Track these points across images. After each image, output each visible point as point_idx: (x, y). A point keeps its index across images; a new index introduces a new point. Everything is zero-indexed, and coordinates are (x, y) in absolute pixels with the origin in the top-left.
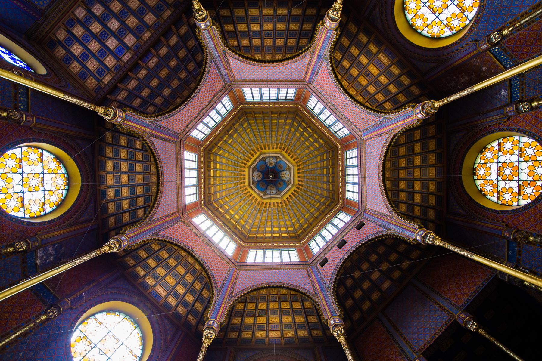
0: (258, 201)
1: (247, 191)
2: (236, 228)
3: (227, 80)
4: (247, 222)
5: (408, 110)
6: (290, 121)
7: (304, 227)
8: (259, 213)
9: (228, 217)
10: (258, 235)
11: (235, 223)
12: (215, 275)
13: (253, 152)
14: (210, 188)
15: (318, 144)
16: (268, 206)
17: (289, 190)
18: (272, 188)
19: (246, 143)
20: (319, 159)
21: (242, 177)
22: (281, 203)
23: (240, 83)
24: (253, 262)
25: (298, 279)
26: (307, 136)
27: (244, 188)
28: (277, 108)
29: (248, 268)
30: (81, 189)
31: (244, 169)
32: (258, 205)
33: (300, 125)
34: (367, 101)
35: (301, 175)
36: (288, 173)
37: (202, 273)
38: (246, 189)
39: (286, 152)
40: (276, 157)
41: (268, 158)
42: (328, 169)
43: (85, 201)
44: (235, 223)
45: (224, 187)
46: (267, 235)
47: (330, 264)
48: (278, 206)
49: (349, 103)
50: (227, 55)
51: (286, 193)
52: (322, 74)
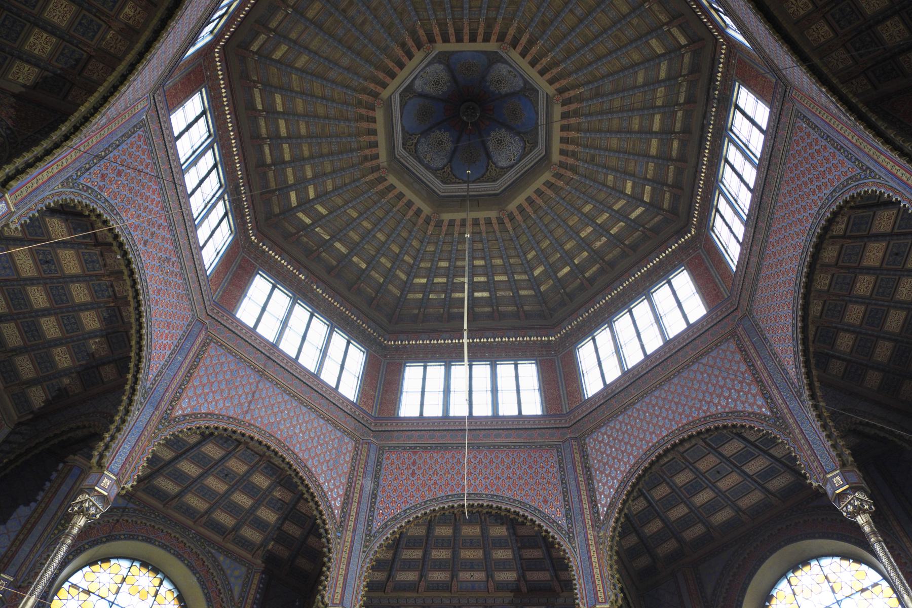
0: (566, 108)
2: (690, 100)
3: (372, 456)
4: (652, 83)
8: (598, 74)
11: (680, 114)
16: (555, 71)
18: (499, 82)
20: (302, 61)
22: (514, 44)
23: (350, 424)
26: (286, 146)
30: (802, 539)
32: (579, 99)
35: (391, 65)
36: (418, 83)
43: (823, 519)
44: (680, 114)
48: (531, 43)
50: (338, 520)
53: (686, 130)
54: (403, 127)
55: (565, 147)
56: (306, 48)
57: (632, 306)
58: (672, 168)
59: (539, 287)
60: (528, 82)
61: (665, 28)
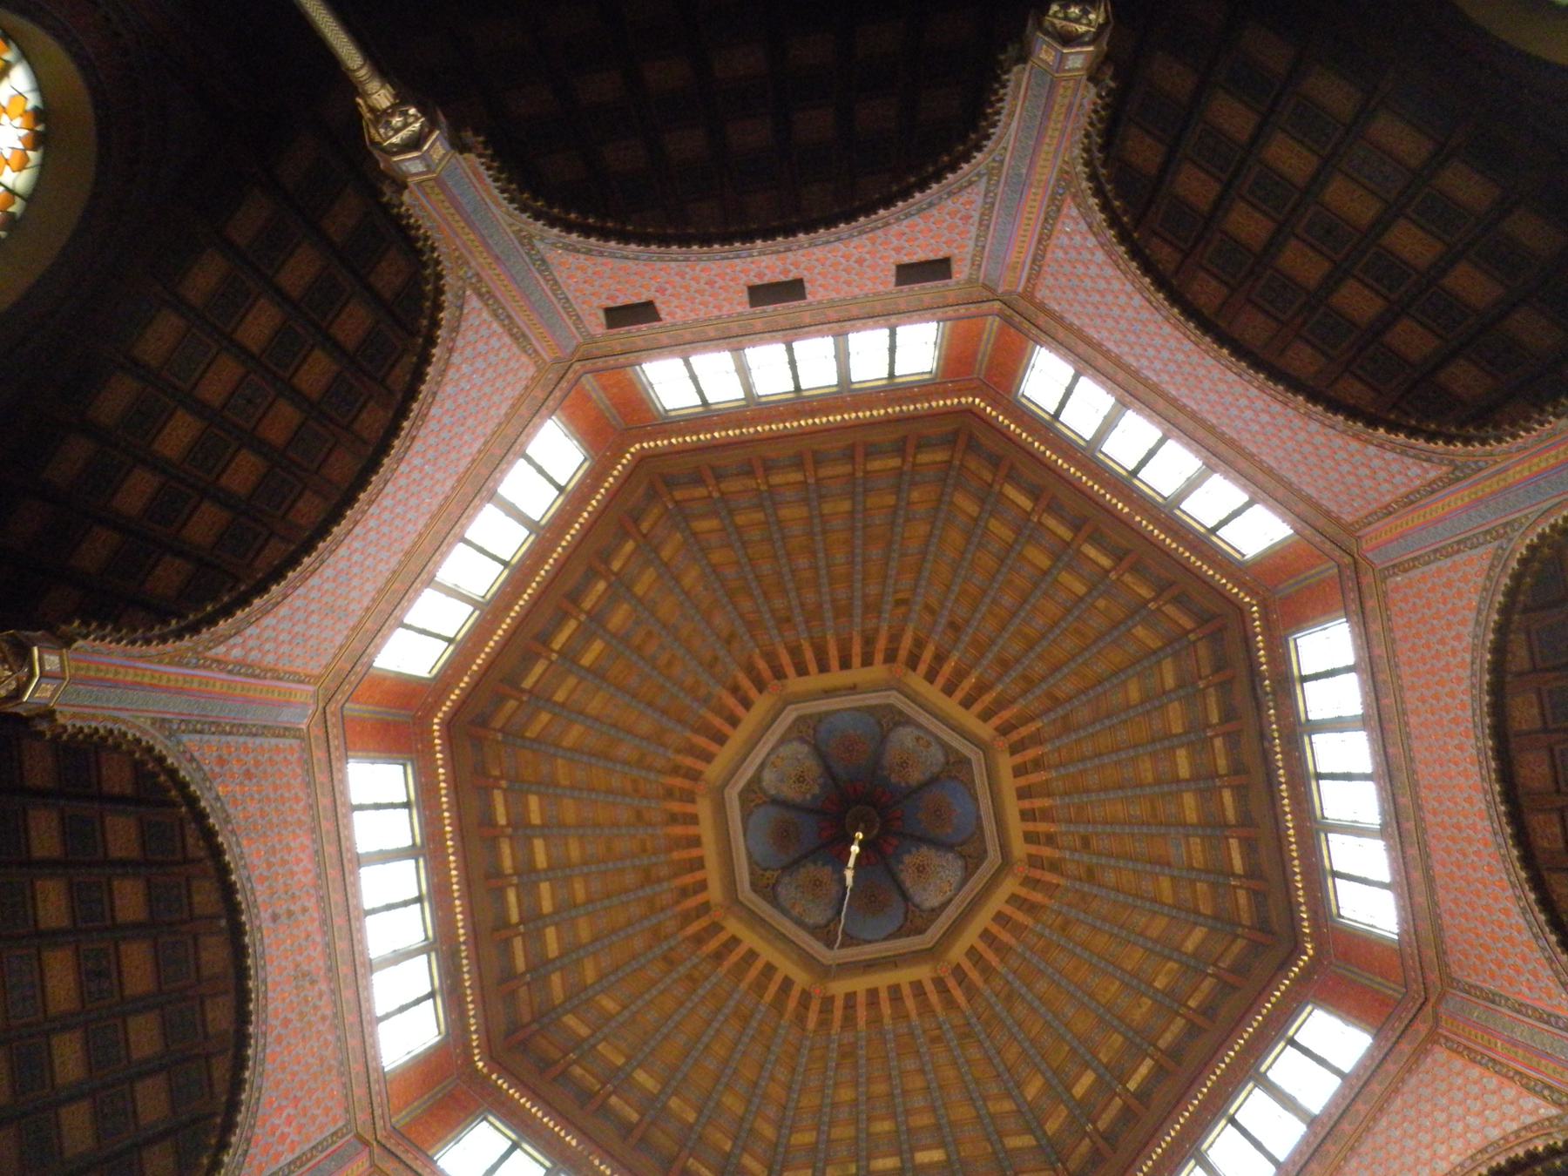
0: (1018, 759)
1: (1033, 849)
2: (1228, 714)
5: (74, 716)
6: (570, 1020)
7: (895, 462)
8: (1060, 695)
9: (1227, 796)
10: (1145, 592)
11: (1218, 742)
12: (1471, 615)
13: (862, 1013)
14: (1208, 1010)
15: (526, 806)
16: (988, 698)
17: (828, 693)
18: (904, 764)
19: (856, 1084)
21: (1005, 936)
22: (913, 663)
24: (1258, 510)
25: (1102, 293)
27: (1038, 874)
28: (583, 1133)
29: (1302, 507)
31: (967, 965)
32: (1036, 739)
33: (540, 966)
34: (186, 861)
35: (717, 722)
37: (1527, 666)
38: (1034, 861)
39: (702, 886)
40: (772, 898)
41: (810, 921)
42: (570, 656)
44: (1218, 742)
45: (1133, 959)
46: (1105, 562)
47: (898, 250)
49: (265, 915)
51: (853, 689)
52: (283, 1137)
53: (1237, 768)
54: (750, 855)
55: (1030, 826)
56: (581, 713)
57: (1124, 473)
58: (1234, 843)
59: (1041, 1125)
60: (951, 747)
61: (1152, 606)
